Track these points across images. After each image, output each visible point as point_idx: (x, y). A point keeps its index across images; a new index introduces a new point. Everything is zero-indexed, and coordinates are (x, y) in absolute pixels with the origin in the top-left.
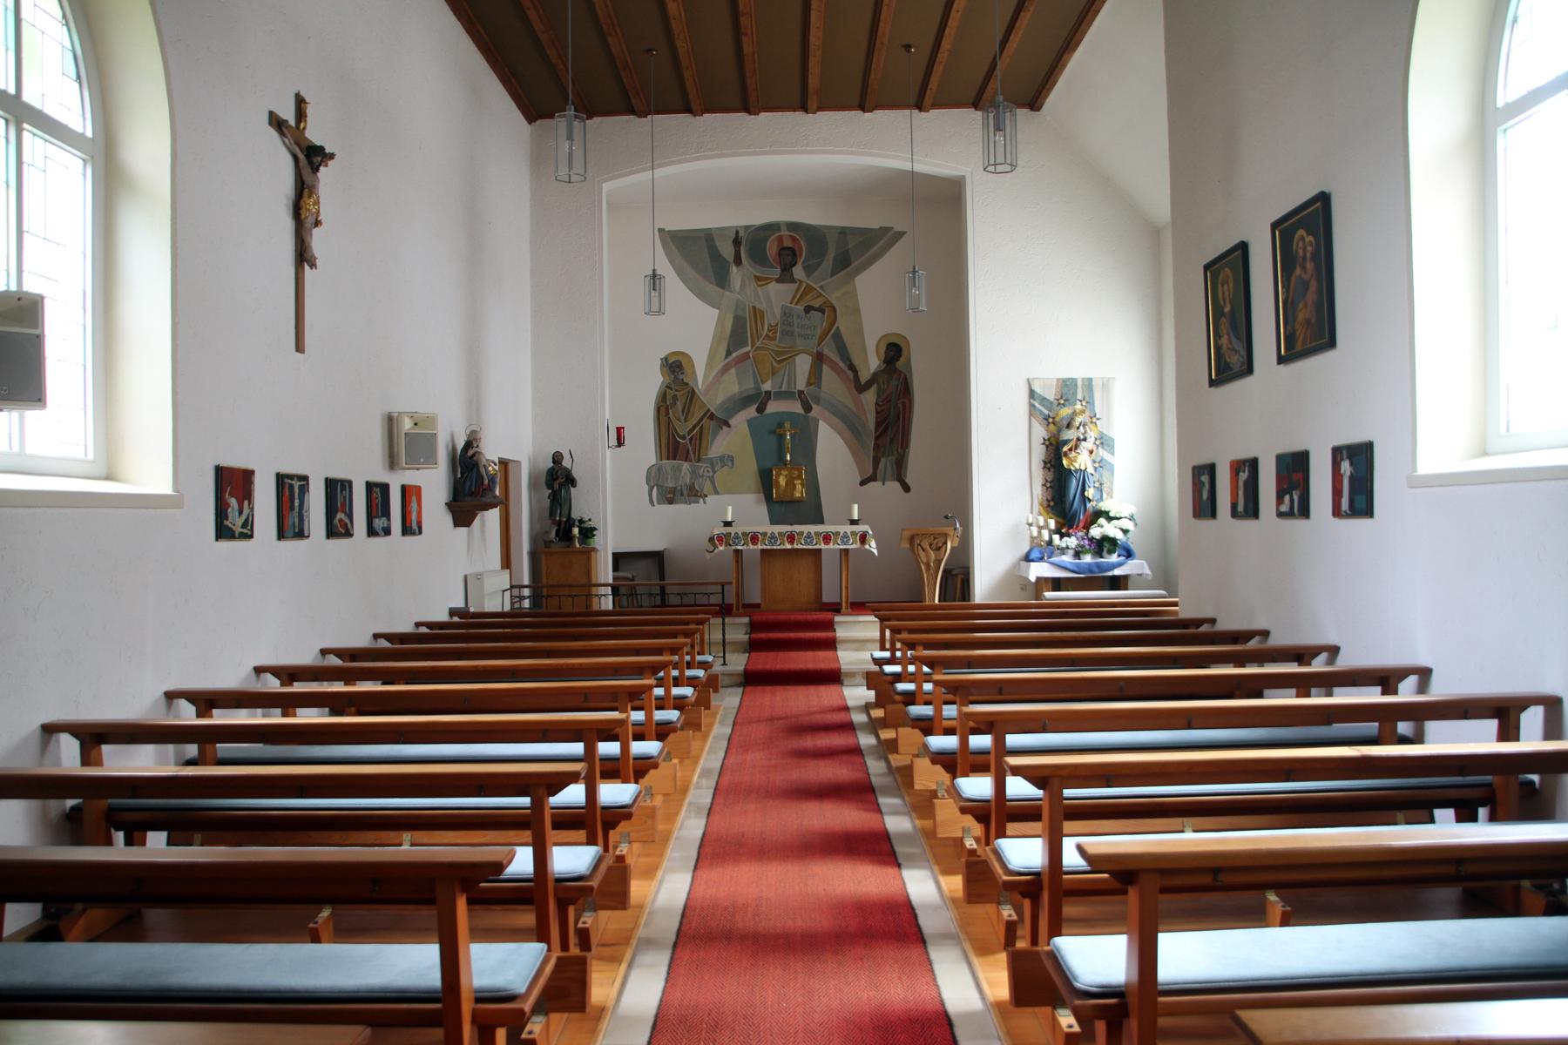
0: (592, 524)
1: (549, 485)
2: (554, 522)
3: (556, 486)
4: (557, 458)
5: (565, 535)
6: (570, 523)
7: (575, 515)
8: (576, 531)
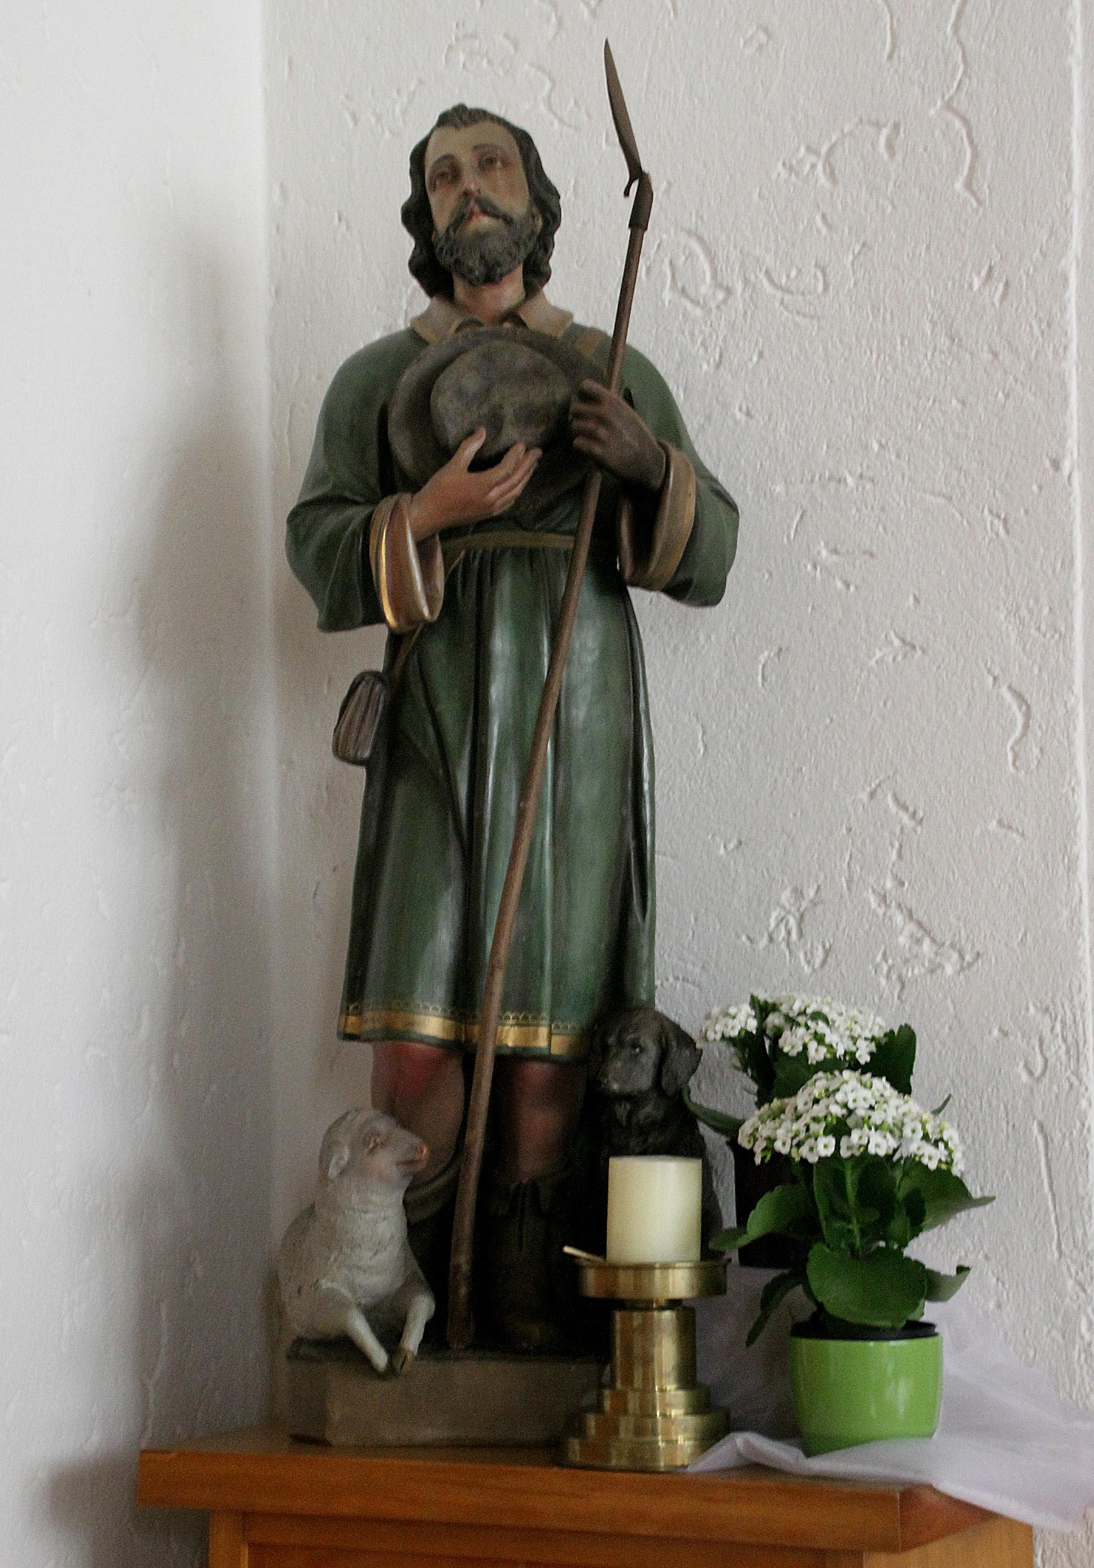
0: (887, 1122)
1: (342, 589)
2: (401, 1093)
3: (410, 577)
4: (475, 210)
5: (512, 1262)
6: (623, 1084)
7: (701, 977)
8: (655, 1207)
